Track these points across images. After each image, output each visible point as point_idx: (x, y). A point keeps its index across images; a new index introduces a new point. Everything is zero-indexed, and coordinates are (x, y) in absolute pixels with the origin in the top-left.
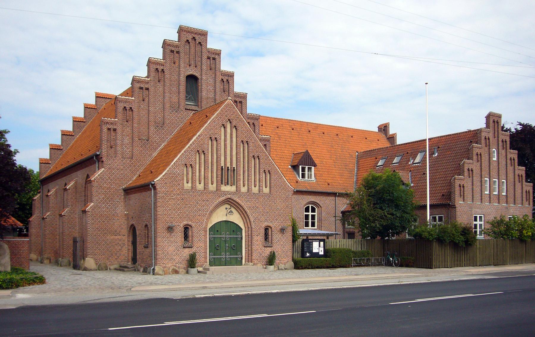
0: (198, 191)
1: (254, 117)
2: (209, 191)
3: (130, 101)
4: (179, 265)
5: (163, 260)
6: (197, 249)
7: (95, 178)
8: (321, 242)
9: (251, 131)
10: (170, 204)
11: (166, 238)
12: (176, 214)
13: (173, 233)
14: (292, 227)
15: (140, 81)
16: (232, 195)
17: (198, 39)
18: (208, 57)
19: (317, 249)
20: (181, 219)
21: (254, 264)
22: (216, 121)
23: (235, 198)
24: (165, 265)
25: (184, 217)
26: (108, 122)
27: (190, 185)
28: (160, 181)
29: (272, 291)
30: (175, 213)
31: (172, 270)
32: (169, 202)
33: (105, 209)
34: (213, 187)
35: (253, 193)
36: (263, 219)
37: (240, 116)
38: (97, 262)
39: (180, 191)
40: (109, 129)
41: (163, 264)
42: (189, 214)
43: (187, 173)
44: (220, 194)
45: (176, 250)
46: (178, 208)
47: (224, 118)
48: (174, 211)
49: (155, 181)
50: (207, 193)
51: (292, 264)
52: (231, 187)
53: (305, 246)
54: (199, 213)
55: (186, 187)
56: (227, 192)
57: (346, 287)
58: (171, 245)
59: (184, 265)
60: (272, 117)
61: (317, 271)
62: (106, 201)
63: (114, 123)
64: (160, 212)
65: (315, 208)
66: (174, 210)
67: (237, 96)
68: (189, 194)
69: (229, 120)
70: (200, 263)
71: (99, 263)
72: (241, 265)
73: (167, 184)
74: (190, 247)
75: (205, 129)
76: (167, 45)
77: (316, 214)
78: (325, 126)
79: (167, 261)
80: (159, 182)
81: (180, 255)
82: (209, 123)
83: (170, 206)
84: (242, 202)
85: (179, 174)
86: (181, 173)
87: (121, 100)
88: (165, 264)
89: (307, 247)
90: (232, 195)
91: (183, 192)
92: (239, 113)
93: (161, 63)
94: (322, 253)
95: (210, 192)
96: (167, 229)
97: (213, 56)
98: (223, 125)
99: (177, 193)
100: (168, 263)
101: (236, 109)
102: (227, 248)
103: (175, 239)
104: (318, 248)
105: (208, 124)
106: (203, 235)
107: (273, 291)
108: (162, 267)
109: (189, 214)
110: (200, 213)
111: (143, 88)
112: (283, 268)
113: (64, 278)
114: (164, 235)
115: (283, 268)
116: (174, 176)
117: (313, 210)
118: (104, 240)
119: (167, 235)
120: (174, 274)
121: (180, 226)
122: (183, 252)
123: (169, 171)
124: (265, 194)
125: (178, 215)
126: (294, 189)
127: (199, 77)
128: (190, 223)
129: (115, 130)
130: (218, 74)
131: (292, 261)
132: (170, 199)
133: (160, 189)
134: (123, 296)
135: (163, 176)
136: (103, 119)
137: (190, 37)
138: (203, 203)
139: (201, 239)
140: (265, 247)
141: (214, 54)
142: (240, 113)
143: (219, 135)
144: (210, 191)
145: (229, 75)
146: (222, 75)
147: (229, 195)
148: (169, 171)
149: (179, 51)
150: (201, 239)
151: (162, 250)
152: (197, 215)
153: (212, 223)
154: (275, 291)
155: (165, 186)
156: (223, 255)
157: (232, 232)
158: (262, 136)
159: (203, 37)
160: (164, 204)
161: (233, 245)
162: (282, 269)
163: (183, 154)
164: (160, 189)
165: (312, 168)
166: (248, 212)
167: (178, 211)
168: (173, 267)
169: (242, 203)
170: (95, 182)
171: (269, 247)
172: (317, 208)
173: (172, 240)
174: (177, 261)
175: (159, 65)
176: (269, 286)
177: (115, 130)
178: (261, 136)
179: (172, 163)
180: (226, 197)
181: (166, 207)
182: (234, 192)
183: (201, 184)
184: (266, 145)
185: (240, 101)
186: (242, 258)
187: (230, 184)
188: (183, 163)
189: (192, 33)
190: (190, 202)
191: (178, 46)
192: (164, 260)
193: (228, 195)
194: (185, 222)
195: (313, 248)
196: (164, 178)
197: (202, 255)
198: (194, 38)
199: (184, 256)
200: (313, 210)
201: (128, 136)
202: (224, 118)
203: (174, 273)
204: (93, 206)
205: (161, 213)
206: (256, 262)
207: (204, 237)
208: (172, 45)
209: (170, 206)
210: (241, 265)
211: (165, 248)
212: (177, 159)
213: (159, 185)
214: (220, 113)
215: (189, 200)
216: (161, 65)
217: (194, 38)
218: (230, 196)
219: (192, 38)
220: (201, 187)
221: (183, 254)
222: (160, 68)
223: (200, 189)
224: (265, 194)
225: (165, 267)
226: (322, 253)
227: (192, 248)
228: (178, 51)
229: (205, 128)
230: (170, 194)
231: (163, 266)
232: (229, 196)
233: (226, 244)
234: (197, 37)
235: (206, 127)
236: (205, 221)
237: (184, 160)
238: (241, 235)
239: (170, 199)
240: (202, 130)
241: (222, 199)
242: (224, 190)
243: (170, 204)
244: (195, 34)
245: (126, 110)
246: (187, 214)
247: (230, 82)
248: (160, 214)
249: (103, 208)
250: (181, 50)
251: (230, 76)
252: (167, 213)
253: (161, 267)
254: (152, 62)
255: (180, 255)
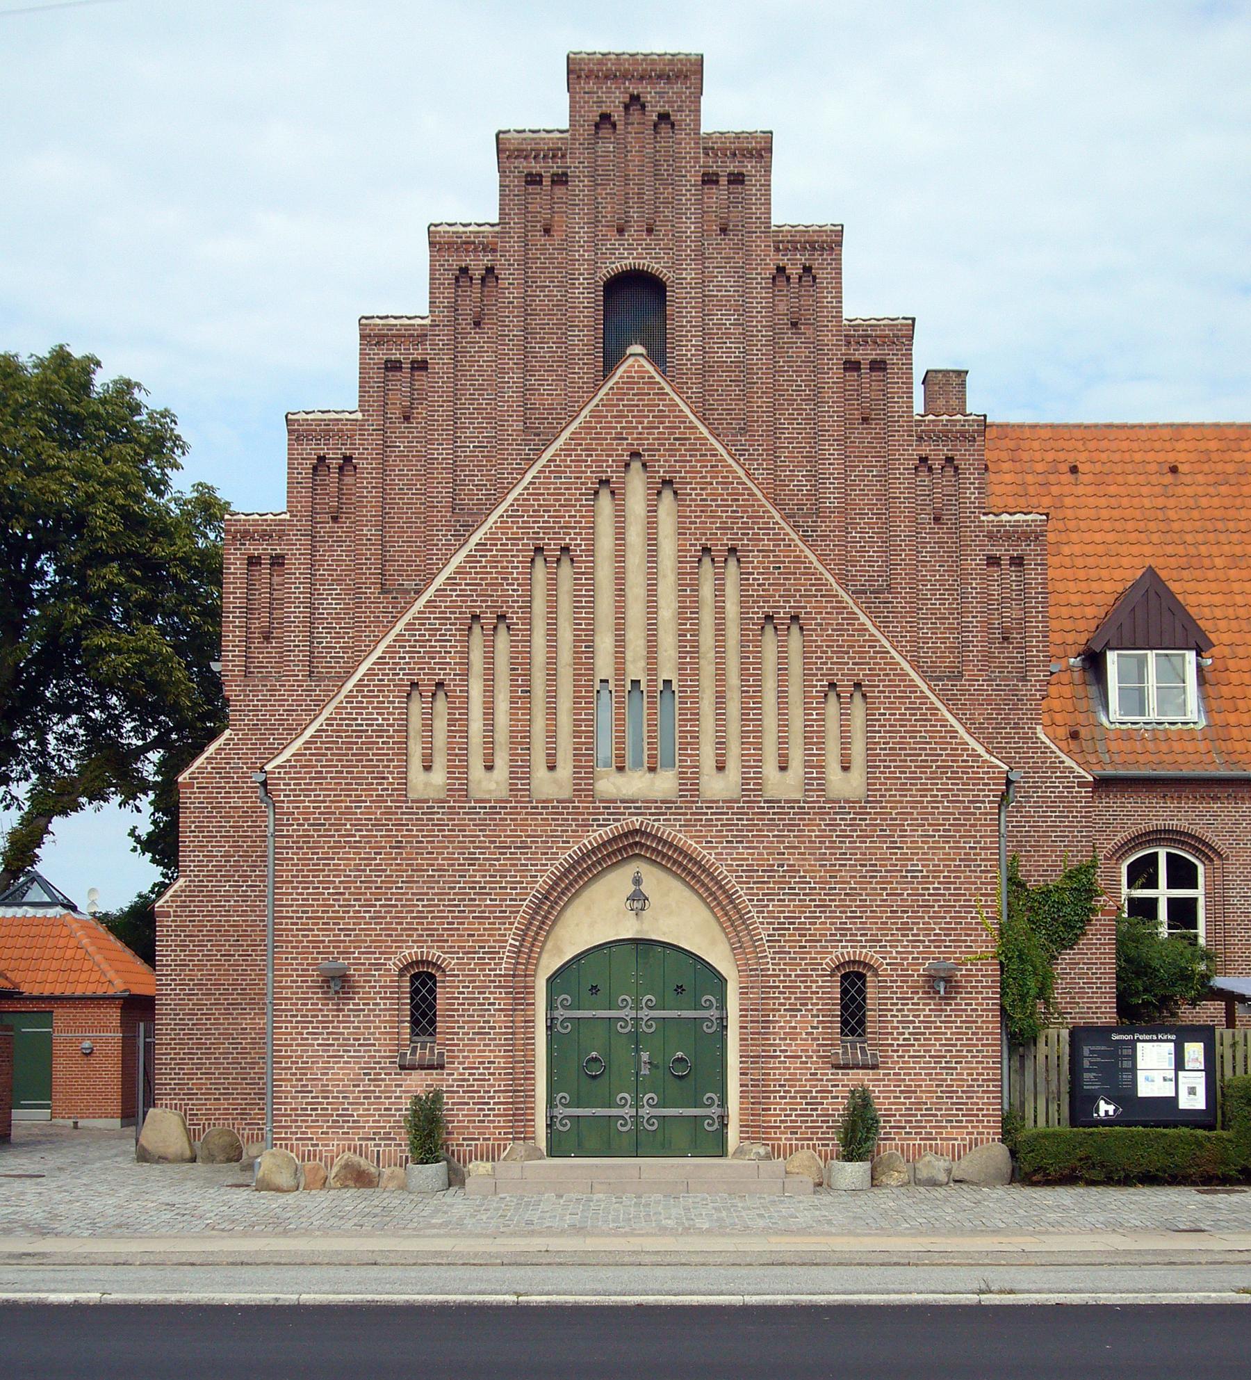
0: (473, 804)
1: (933, 431)
2: (531, 802)
3: (342, 431)
4: (380, 1145)
5: (302, 1121)
6: (470, 1074)
7: (193, 773)
8: (1172, 1044)
9: (753, 495)
10: (337, 871)
11: (318, 1022)
12: (367, 915)
13: (955, 998)
14: (1001, 963)
15: (387, 336)
16: (651, 814)
17: (655, 98)
18: (704, 175)
19: (1165, 1079)
20: (391, 935)
21: (776, 1152)
22: (570, 467)
23: (668, 830)
24: (313, 1145)
25: (404, 926)
26: (247, 531)
27: (439, 777)
28: (291, 767)
29: (42, 1295)
30: (359, 912)
31: (343, 1172)
32: (333, 859)
33: (232, 903)
34: (555, 781)
35: (766, 802)
36: (823, 925)
37: (696, 428)
38: (197, 1127)
39: (386, 807)
40: (253, 561)
41: (300, 1142)
42: (429, 912)
43: (428, 727)
44: (589, 814)
45: (363, 1080)
46: (377, 888)
47: (609, 451)
48: (355, 900)
49: (268, 768)
50: (519, 814)
51: (1000, 1152)
52: (649, 776)
53: (1086, 1064)
54: (479, 906)
55: (420, 787)
56: (642, 802)
57: (544, 1298)
58: (342, 1057)
59: (401, 1145)
60: (1161, 422)
61: (1065, 1196)
62: (237, 865)
63: (274, 531)
64: (292, 906)
65: (1193, 863)
66: (358, 895)
67: (862, 336)
68: (428, 820)
69: (635, 455)
70: (484, 1139)
71: (207, 1131)
72: (723, 1154)
73: (326, 778)
74: (431, 1067)
75: (513, 513)
76: (508, 157)
77: (1199, 893)
78: (1143, 431)
79: (322, 1127)
80: (285, 773)
81: (384, 1104)
82: (530, 483)
83: (337, 880)
84: (703, 848)
85: (380, 732)
86: (393, 725)
87: (306, 431)
88: (311, 1139)
89: (1101, 1068)
90: (651, 814)
91: (403, 813)
92: (687, 417)
93: (482, 243)
94: (1198, 1102)
95: (536, 808)
96: (323, 981)
97: (732, 167)
98: (601, 482)
99: (371, 819)
100: (328, 1139)
101: (672, 400)
102: (645, 1071)
103: (359, 1028)
104: (1171, 1074)
105: (526, 488)
106: (501, 1010)
107: (53, 1298)
108: (297, 1156)
109: (429, 912)
110: (486, 906)
111: (400, 362)
112: (943, 1177)
113: (23, 1193)
114: (308, 1010)
115: (943, 1177)
116: (357, 743)
117: (1182, 874)
118: (227, 1035)
119: (321, 1010)
120: (346, 1187)
121: (386, 970)
122: (401, 1086)
123: (335, 719)
124: (834, 802)
125: (377, 918)
126: (1007, 768)
127: (666, 275)
128: (435, 953)
129: (278, 561)
130: (760, 246)
131: (1003, 1141)
132: (337, 846)
133: (289, 802)
134: (1221, 1263)
135: (307, 742)
136: (228, 520)
137: (614, 100)
138: (498, 860)
139: (490, 1028)
140: (837, 1067)
141: (735, 155)
142: (692, 417)
143: (580, 534)
144: (600, 801)
145: (812, 243)
146: (777, 250)
147: (634, 818)
148: (335, 719)
149: (565, 174)
150: (490, 1028)
151: (297, 1080)
152: (467, 918)
153: (559, 951)
154: (67, 1298)
155: (315, 790)
156: (624, 1106)
157: (670, 994)
158: (997, 519)
159: (678, 87)
160: (309, 871)
161: (680, 1054)
162: (933, 1183)
163: (399, 638)
164: (289, 802)
165: (1187, 658)
166: (741, 893)
167: (376, 900)
168: (347, 1155)
169: (705, 852)
170: (195, 790)
171: (858, 1068)
172: (1203, 862)
173: (346, 1031)
174: (370, 1127)
175: (475, 250)
176: (555, 1267)
177: (278, 561)
178: (991, 517)
179: (350, 685)
180: (618, 824)
181: (319, 882)
182: (662, 802)
183: (496, 772)
184: (1021, 558)
185: (873, 362)
186: (723, 1121)
187: (646, 765)
188: (402, 680)
189: (626, 76)
190: (437, 859)
191: (561, 149)
192: (306, 1121)
193: (630, 814)
194: (412, 947)
195: (1141, 1076)
196: (311, 755)
197: (495, 1103)
198: (635, 99)
199: (404, 1107)
200: (1182, 874)
201: (339, 581)
202: (609, 451)
203: (351, 1183)
204: (182, 891)
205: (297, 912)
206: (784, 1139)
207: (503, 1018)
208: (532, 150)
209: (339, 876)
210: (723, 1154)
211: (311, 1068)
212: (375, 663)
213: (289, 785)
214: (587, 428)
215: (429, 845)
216: (484, 250)
217: (635, 100)
218: (641, 818)
219: (627, 100)
220: (493, 786)
221: (400, 1097)
222: (477, 265)
223: (490, 792)
224: (834, 802)
225: (311, 1156)
226: (1193, 1099)
227: (445, 1072)
228: (560, 171)
229: (512, 505)
230: (338, 825)
231: (301, 1148)
232: (636, 822)
233: (637, 1050)
234: (649, 93)
235: (516, 500)
236: (511, 941)
237: (409, 663)
238: (723, 1005)
239: (337, 846)
240: (494, 517)
241: (596, 834)
242: (615, 791)
243: (337, 871)
244: (642, 78)
245: (930, 469)
246: (419, 912)
247: (820, 274)
248: (292, 918)
249: (227, 898)
250: (576, 165)
251: (823, 249)
252: (323, 912)
253: (293, 1155)
254: (440, 243)
255: (384, 1104)
